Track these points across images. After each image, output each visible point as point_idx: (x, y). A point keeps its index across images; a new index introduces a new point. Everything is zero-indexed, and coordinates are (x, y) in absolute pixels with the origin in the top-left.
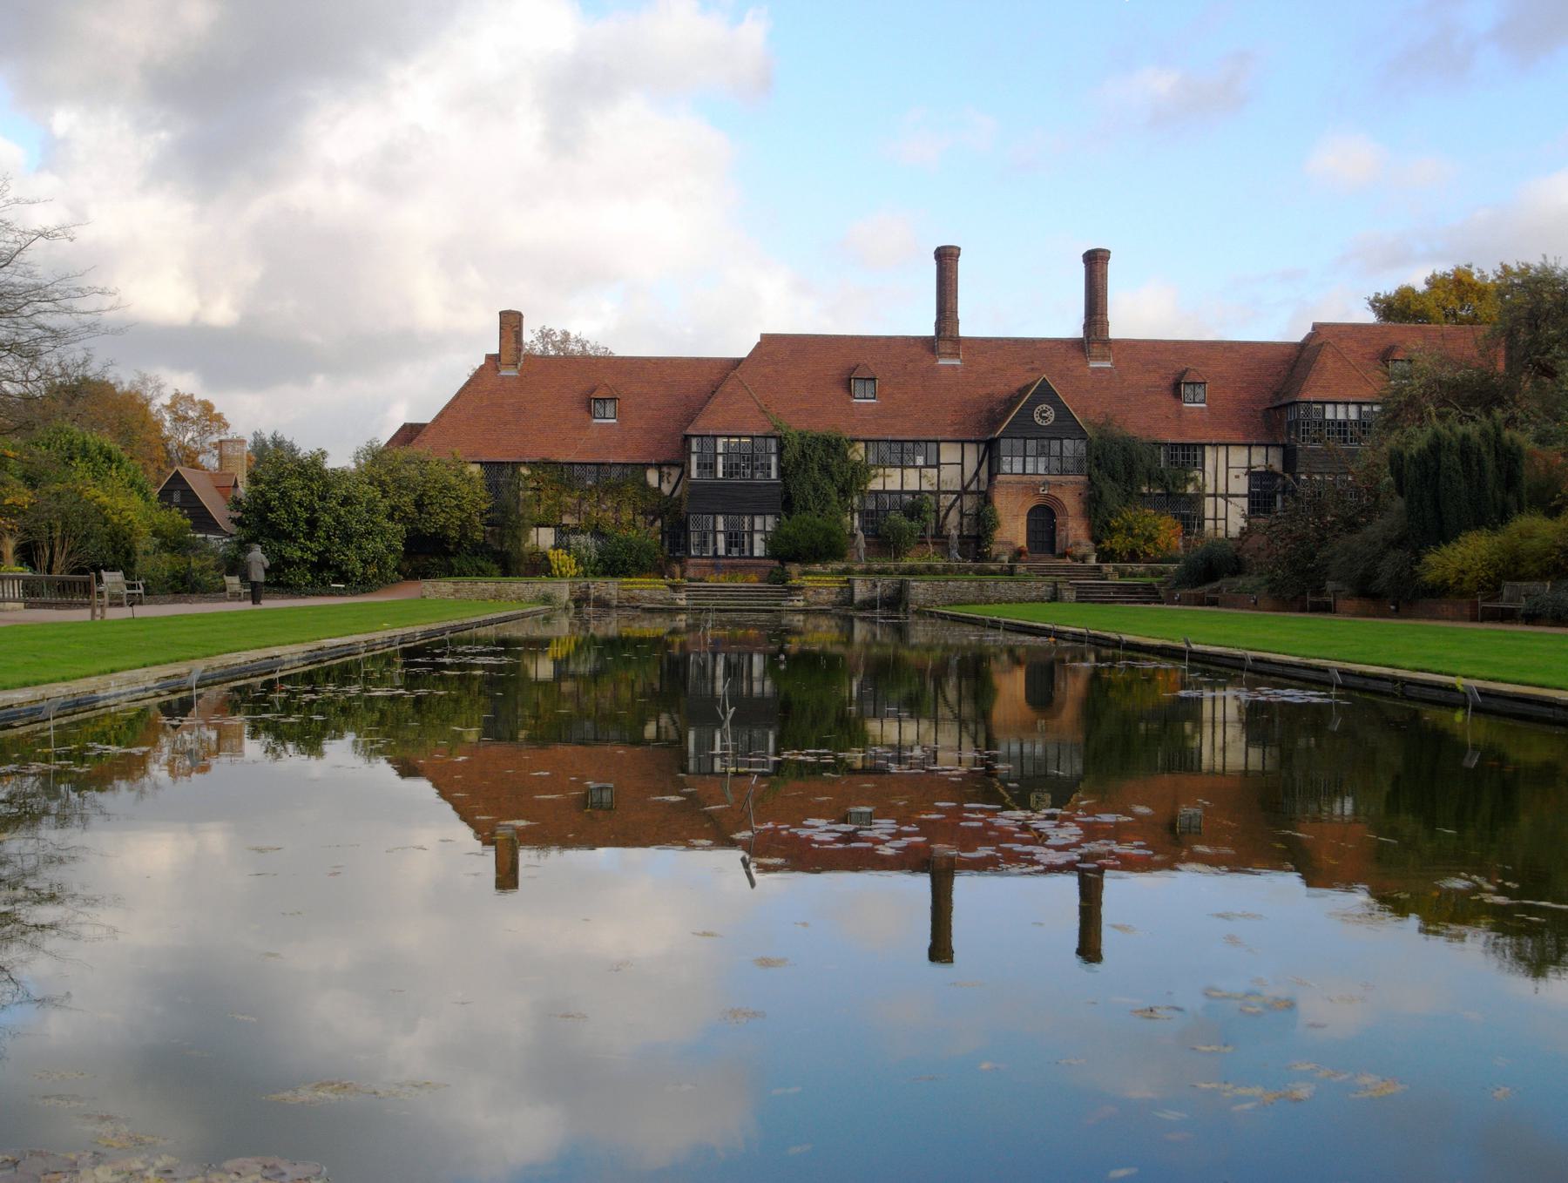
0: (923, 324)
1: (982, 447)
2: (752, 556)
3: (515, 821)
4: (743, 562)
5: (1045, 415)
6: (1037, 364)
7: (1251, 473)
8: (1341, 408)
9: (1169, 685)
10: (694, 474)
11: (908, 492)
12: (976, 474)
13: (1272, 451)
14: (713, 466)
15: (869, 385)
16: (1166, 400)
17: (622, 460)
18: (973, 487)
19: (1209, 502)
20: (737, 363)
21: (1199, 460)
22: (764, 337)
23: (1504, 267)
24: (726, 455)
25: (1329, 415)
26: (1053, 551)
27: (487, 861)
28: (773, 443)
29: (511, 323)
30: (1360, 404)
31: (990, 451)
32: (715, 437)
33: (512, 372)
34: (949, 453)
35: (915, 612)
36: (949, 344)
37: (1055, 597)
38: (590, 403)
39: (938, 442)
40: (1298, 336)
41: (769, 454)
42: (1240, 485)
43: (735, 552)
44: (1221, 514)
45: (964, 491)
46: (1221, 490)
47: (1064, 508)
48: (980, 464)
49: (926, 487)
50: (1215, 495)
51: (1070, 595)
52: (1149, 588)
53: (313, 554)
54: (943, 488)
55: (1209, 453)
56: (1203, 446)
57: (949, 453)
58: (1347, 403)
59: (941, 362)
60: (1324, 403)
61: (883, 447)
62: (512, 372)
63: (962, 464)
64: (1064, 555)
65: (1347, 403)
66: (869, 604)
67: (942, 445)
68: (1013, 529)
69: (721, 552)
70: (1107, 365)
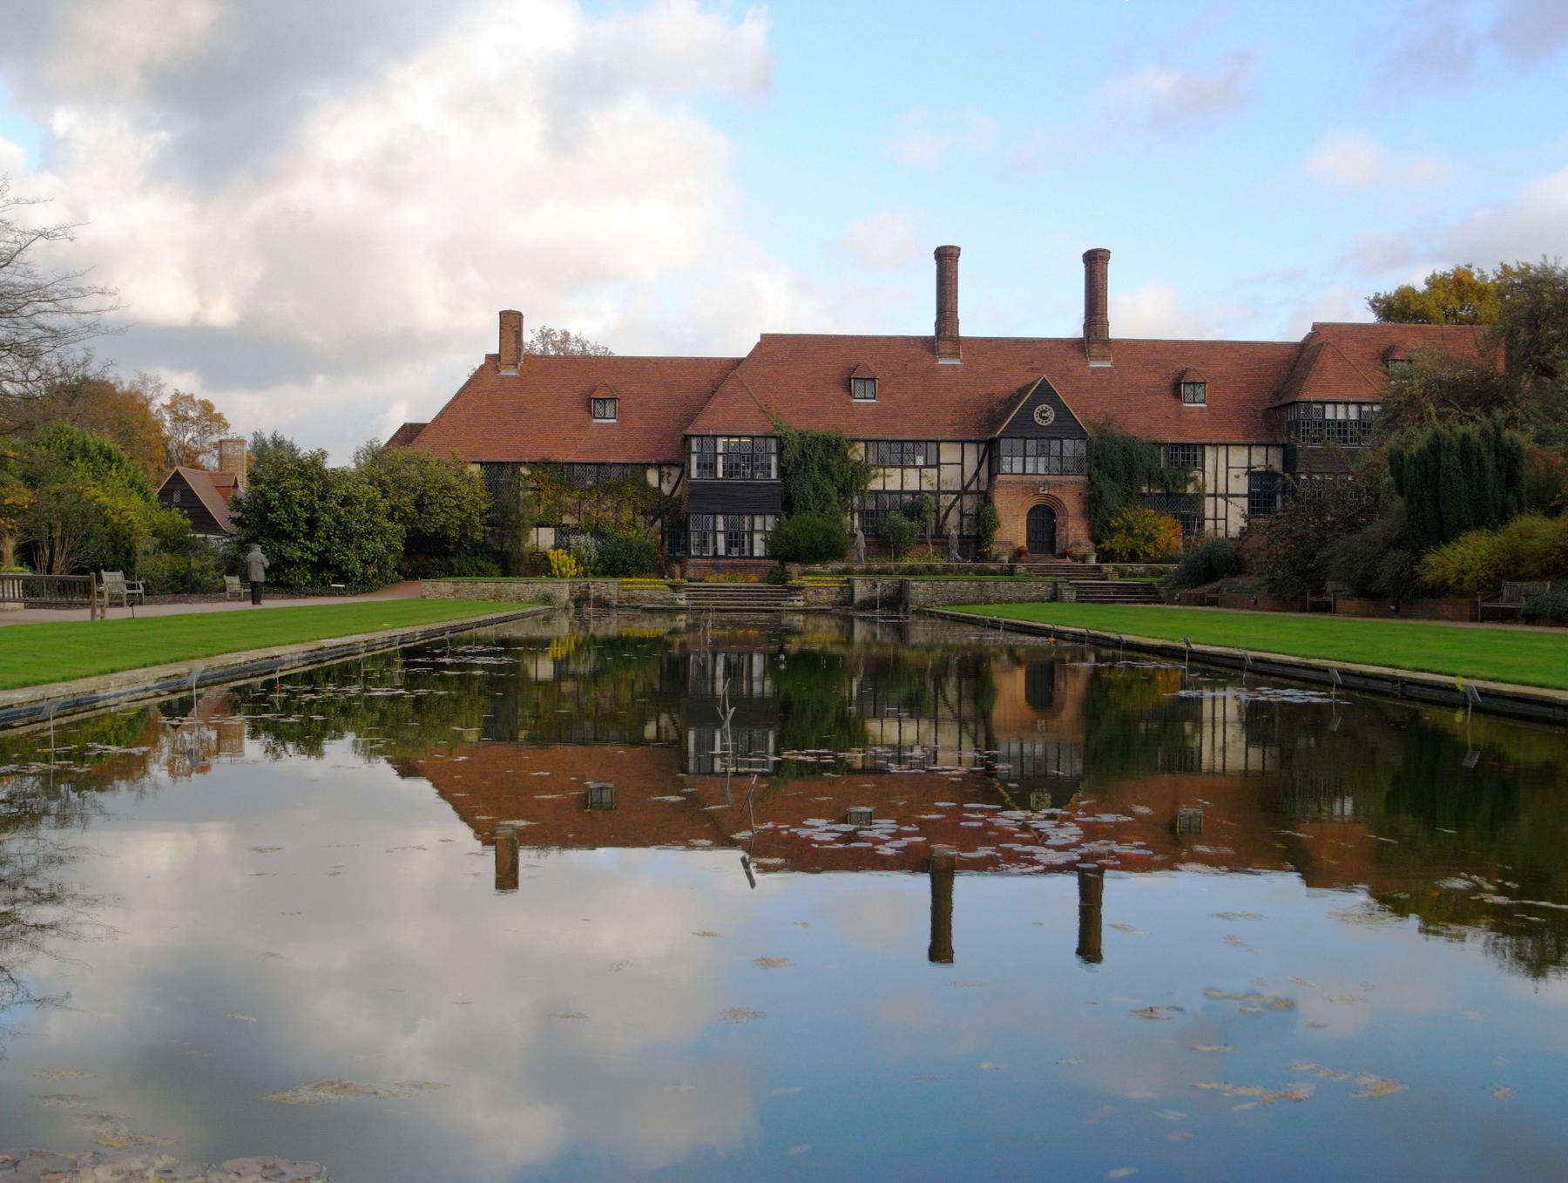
0: (923, 324)
1: (982, 447)
2: (752, 556)
3: (515, 821)
4: (743, 562)
5: (1045, 415)
6: (1037, 364)
7: (1251, 473)
8: (1341, 408)
9: (1169, 685)
10: (694, 474)
11: (908, 492)
12: (976, 474)
13: (1272, 451)
14: (713, 466)
15: (869, 385)
16: (1166, 400)
17: (622, 460)
18: (973, 487)
19: (1209, 502)
20: (737, 363)
21: (1199, 460)
22: (764, 337)
23: (1504, 267)
24: (726, 455)
25: (1329, 415)
26: (1053, 551)
27: (487, 861)
28: (773, 443)
29: (511, 323)
30: (1360, 404)
31: (990, 451)
32: (715, 437)
33: (512, 372)
34: (949, 453)
35: (915, 612)
36: (949, 344)
37: (1055, 597)
38: (590, 403)
39: (938, 442)
40: (1298, 336)
41: (769, 454)
42: (1240, 485)
43: (735, 552)
44: (1221, 514)
45: (964, 491)
46: (1221, 490)
47: (1064, 508)
48: (980, 464)
49: (926, 487)
50: (1215, 495)
51: (1070, 595)
52: (1149, 588)
53: (313, 554)
54: (943, 488)
55: (1209, 453)
56: (1203, 446)
57: (949, 453)
58: (1347, 403)
59: (941, 362)
60: (1324, 403)
61: (883, 447)
62: (512, 372)
63: (962, 464)
64: (1064, 555)
65: (1347, 403)
66: (869, 604)
67: (942, 445)
68: (1013, 529)
69: (721, 552)
70: (1107, 365)
